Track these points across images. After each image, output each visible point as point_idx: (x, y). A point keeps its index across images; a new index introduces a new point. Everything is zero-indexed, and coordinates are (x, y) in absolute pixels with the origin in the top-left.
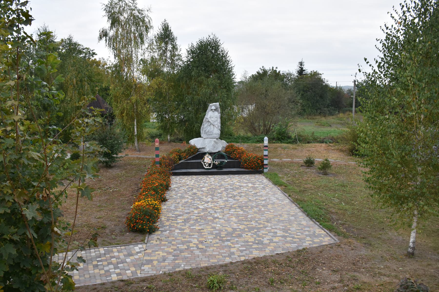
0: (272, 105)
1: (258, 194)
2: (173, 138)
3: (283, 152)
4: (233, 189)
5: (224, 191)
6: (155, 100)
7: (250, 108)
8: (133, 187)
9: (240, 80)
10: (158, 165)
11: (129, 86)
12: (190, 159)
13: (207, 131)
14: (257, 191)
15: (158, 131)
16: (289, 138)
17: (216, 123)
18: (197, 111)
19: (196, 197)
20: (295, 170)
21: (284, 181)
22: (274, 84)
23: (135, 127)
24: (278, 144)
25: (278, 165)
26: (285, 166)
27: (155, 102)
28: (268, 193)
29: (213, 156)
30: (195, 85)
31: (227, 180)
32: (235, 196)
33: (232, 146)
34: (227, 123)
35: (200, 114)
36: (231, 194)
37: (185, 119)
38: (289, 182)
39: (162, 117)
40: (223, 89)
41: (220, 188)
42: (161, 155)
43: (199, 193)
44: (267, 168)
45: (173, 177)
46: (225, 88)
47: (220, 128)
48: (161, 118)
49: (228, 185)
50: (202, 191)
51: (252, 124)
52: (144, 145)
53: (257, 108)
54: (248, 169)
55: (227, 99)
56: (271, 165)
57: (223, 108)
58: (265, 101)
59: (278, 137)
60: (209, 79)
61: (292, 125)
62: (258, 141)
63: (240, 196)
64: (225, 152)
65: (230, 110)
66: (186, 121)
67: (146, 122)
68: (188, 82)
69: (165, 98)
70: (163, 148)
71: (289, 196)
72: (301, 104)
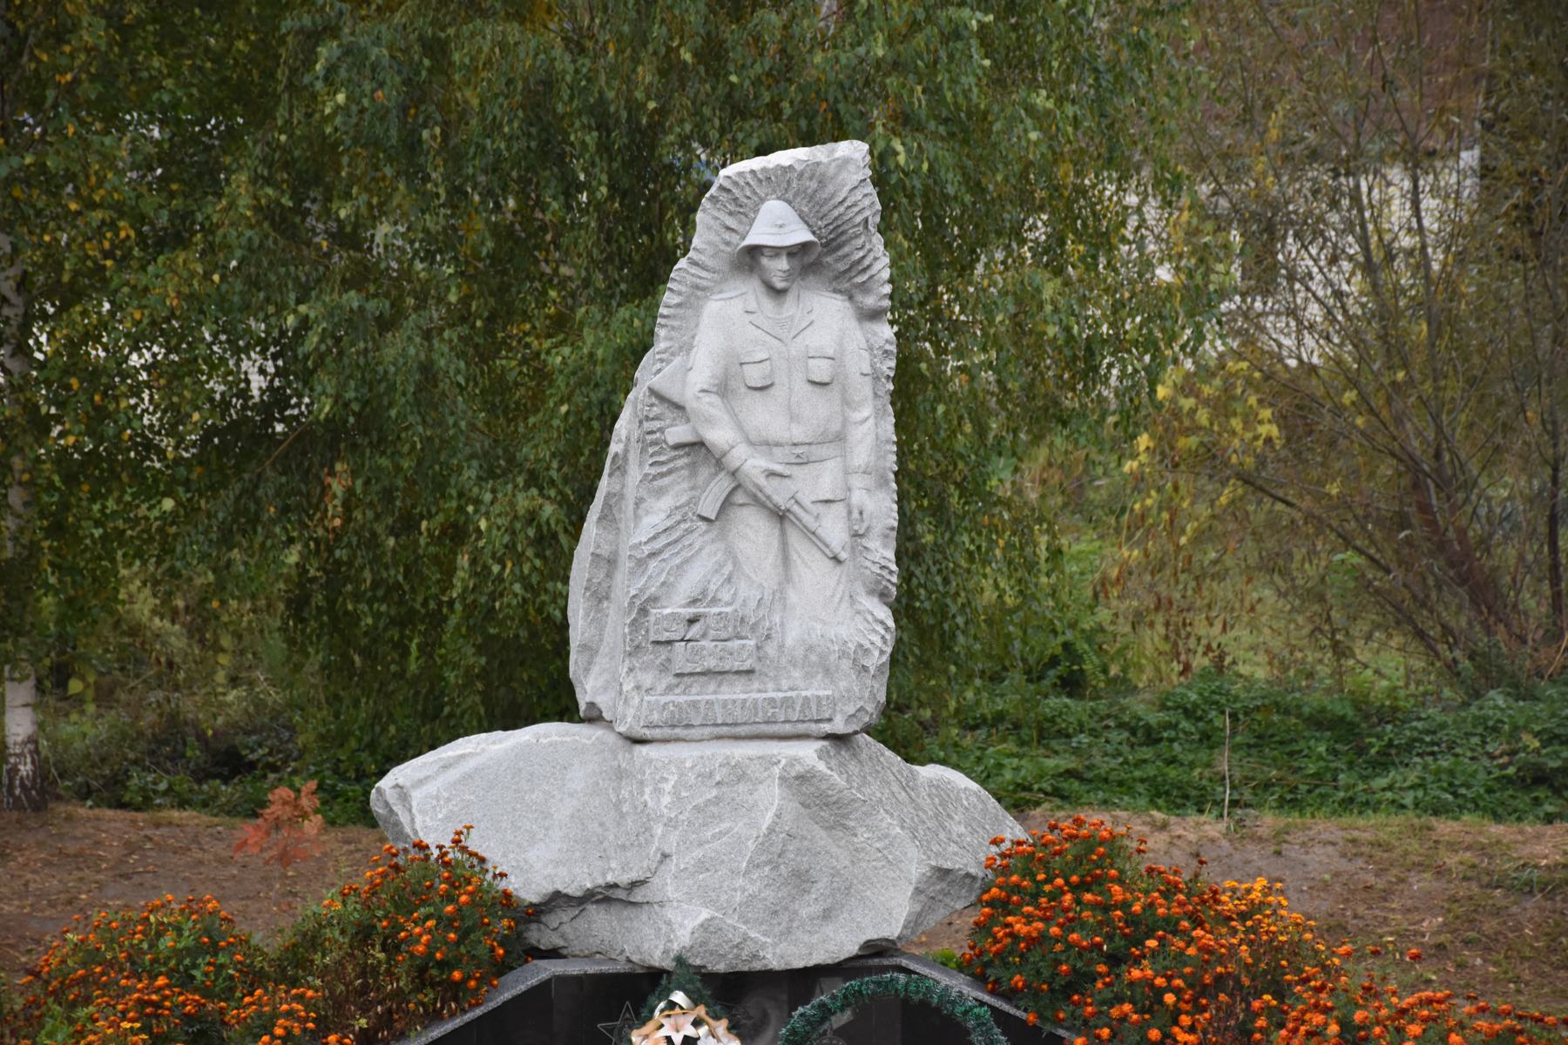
2: (86, 729)
13: (675, 606)
17: (821, 481)
18: (506, 277)
33: (1092, 864)
34: (1001, 479)
35: (561, 325)
37: (316, 404)
51: (1430, 482)
55: (997, 82)
57: (933, 228)
62: (1537, 778)
65: (1052, 257)
66: (320, 444)
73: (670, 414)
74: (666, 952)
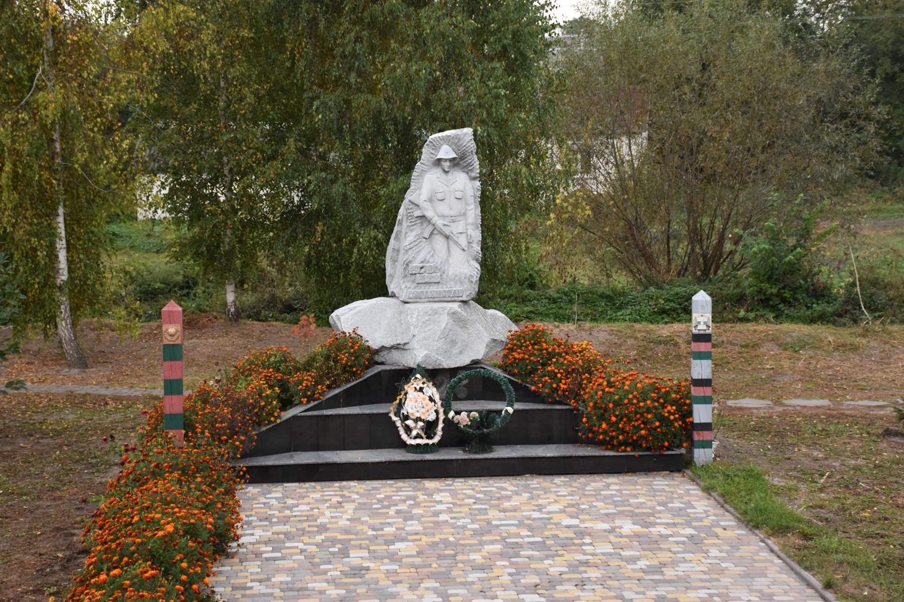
0: (734, 134)
1: (669, 573)
2: (249, 298)
3: (786, 364)
4: (542, 546)
5: (502, 555)
6: (160, 112)
7: (625, 149)
8: (44, 546)
9: (573, 15)
10: (176, 434)
11: (23, 38)
12: (334, 402)
13: (417, 263)
14: (664, 556)
15: (175, 266)
16: (820, 293)
19: (361, 590)
20: (855, 455)
21: (798, 507)
22: (742, 30)
23: (61, 245)
24: (761, 327)
25: (762, 427)
26: (798, 432)
27: (160, 124)
28: (716, 570)
29: (446, 386)
30: (358, 39)
31: (515, 502)
32: (552, 583)
33: (537, 338)
34: (512, 226)
35: (384, 182)
36: (537, 572)
38: (823, 513)
39: (197, 197)
40: (491, 60)
41: (482, 543)
42: (194, 380)
43: (379, 569)
44: (707, 444)
45: (252, 490)
46: (503, 54)
47: (477, 248)
48: (190, 201)
49: (521, 524)
50: (393, 557)
51: (634, 228)
52: (107, 336)
53: (659, 153)
54: (613, 448)
56: (731, 428)
57: (492, 152)
58: (696, 115)
59: (760, 291)
60: (423, 13)
61: (834, 231)
62: (663, 312)
63: (581, 584)
64: (504, 368)
65: (526, 162)
66: (314, 217)
67: (113, 218)
68: (322, 25)
69: (208, 101)
70: (203, 345)
71: (828, 586)
72: (882, 124)
73: (415, 208)
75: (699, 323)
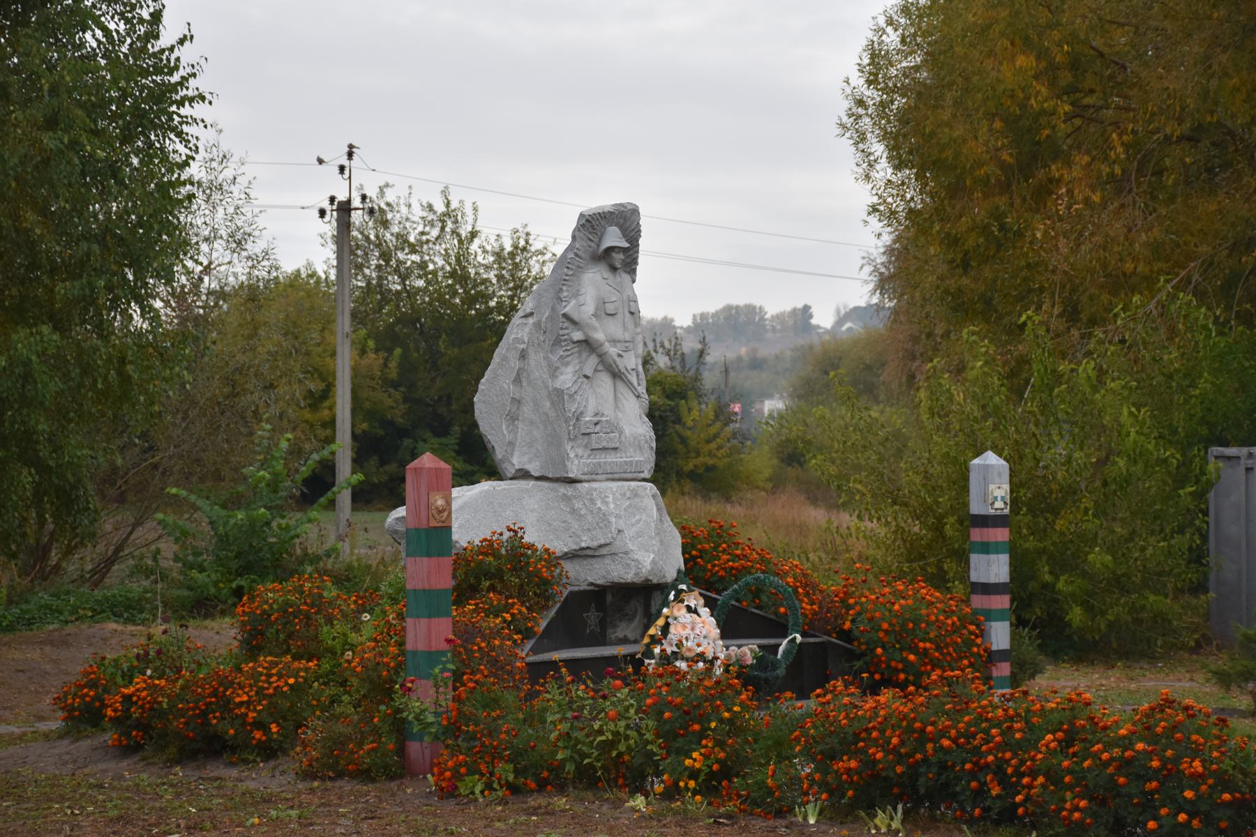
73: (571, 327)
74: (636, 574)
75: (996, 498)
